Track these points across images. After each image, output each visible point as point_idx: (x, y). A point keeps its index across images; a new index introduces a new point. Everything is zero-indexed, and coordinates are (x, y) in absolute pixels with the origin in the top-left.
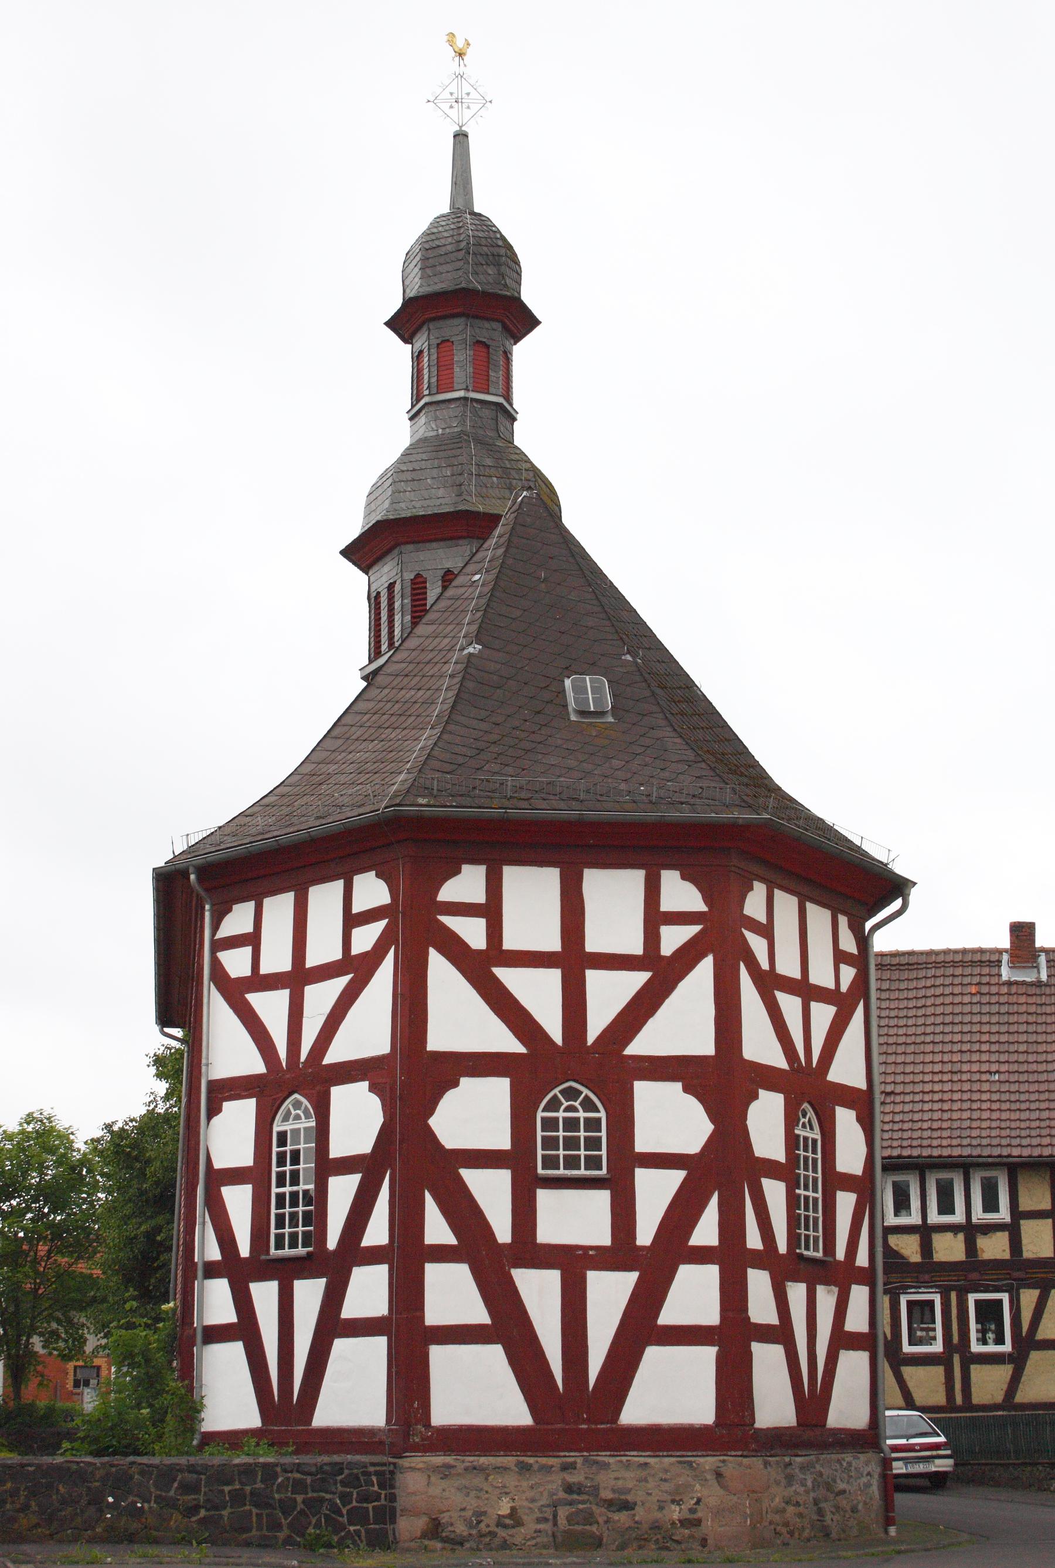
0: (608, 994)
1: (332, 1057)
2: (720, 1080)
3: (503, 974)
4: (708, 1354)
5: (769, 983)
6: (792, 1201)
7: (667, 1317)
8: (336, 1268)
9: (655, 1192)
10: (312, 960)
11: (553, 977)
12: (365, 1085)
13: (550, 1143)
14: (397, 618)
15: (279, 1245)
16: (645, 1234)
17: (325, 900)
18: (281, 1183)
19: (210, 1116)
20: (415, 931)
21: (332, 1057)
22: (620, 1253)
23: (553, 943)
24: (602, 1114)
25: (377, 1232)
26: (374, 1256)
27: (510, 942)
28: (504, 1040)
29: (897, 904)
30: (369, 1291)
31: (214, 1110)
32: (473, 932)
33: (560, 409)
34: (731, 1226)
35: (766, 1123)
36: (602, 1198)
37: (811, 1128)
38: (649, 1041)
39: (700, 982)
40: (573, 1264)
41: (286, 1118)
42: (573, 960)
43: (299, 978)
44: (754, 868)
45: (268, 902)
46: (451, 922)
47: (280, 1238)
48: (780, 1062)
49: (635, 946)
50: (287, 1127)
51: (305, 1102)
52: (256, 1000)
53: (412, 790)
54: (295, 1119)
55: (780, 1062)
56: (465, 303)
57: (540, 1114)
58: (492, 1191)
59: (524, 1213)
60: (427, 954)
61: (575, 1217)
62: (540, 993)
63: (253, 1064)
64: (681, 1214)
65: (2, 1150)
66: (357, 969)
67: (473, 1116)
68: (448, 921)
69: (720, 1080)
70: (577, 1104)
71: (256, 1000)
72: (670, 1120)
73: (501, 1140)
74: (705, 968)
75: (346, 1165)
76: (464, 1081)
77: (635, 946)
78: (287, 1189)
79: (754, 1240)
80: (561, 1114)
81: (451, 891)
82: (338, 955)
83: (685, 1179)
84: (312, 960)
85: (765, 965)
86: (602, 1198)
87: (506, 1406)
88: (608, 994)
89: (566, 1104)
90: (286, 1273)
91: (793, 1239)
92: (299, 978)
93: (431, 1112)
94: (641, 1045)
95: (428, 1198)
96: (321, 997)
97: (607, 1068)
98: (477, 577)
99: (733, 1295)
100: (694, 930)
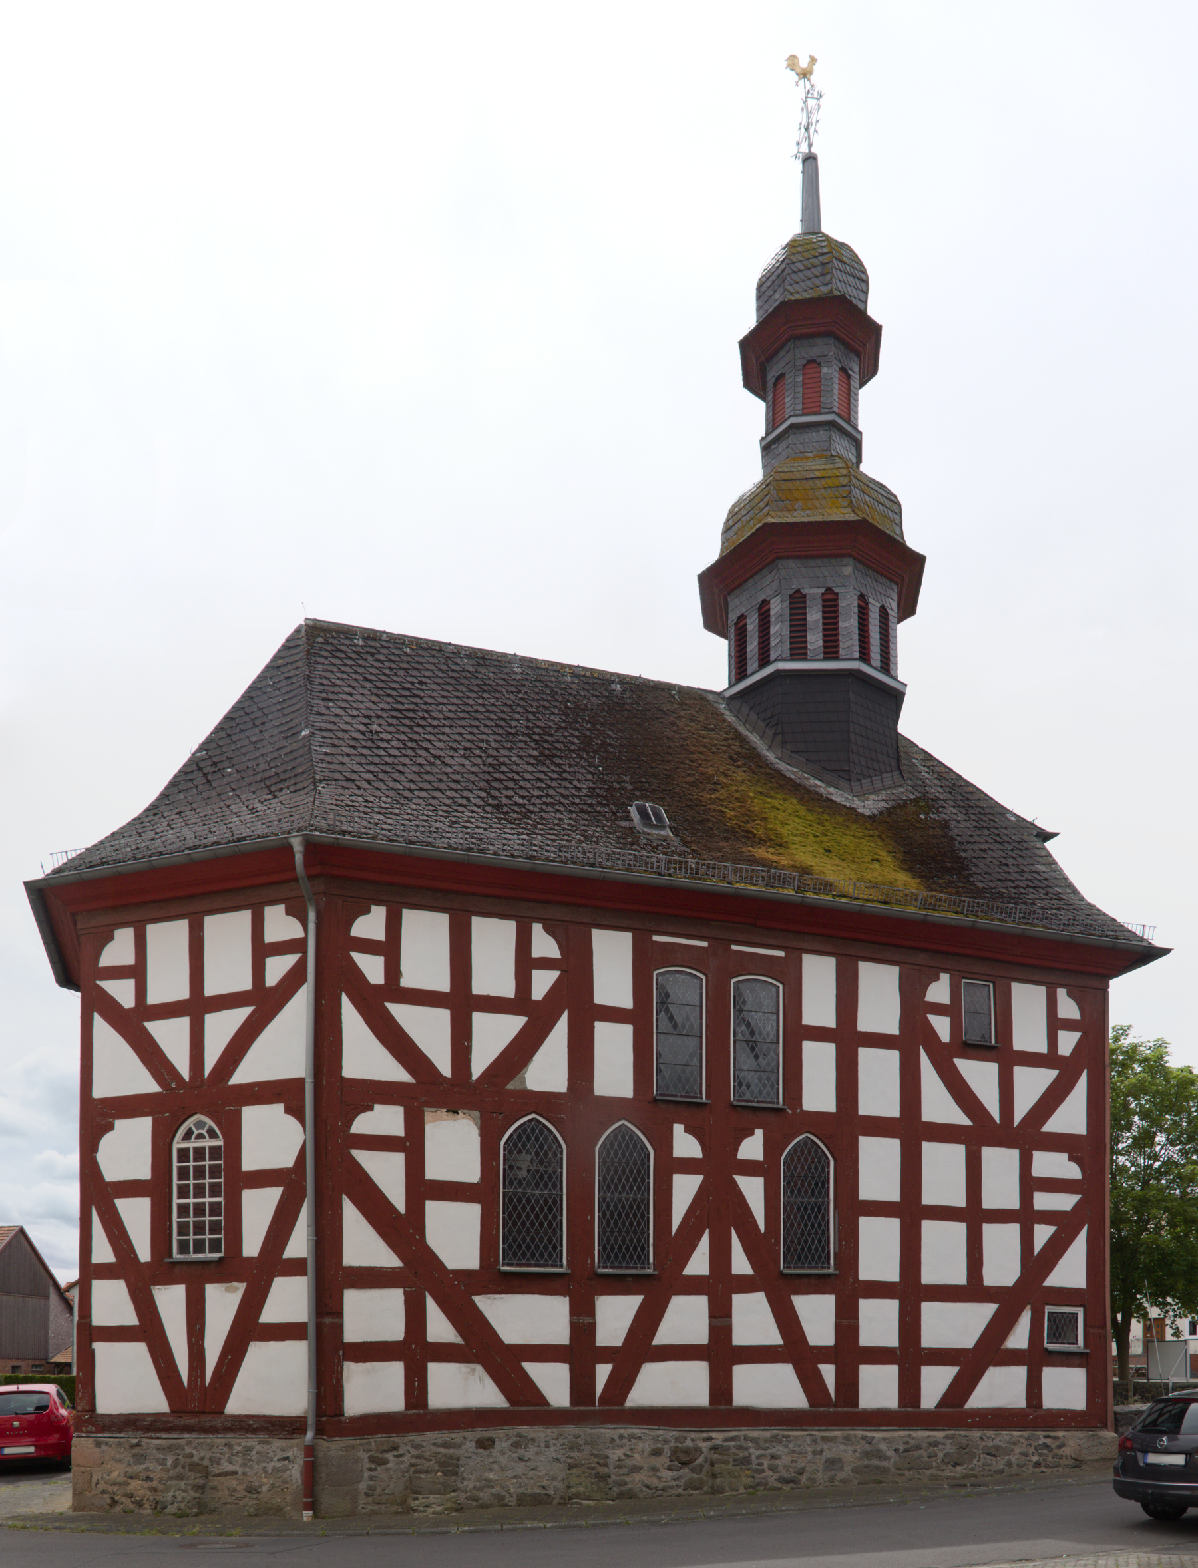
7: (664, 1336)
15: (184, 1247)
17: (228, 934)
18: (184, 1192)
25: (299, 1245)
26: (296, 1268)
30: (289, 1300)
33: (898, 434)
41: (188, 1135)
42: (461, 1002)
43: (197, 1006)
50: (192, 1144)
51: (210, 1123)
52: (156, 1028)
55: (150, 1086)
56: (812, 330)
62: (430, 1030)
65: (1191, 1139)
70: (204, 1132)
73: (143, 1171)
76: (377, 1107)
87: (154, 1400)
88: (492, 1035)
89: (196, 1132)
90: (195, 1280)
92: (197, 1006)
96: (221, 1028)
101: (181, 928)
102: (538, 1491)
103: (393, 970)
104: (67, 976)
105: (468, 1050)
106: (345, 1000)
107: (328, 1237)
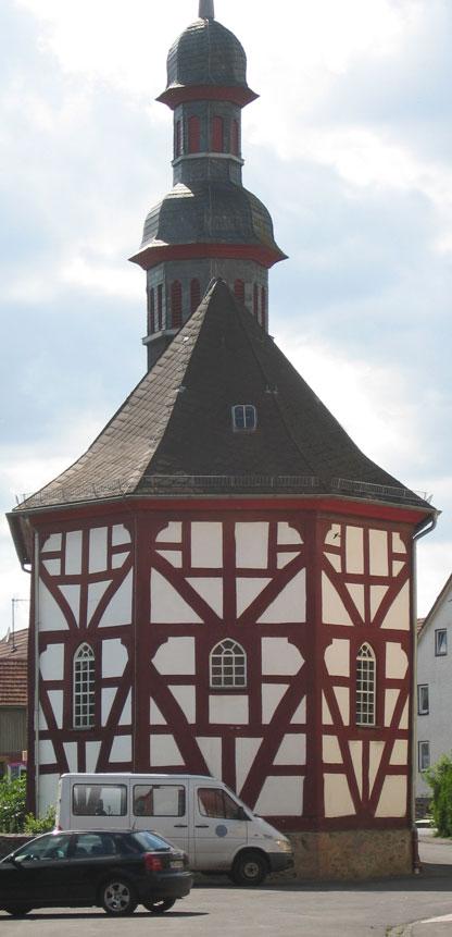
0: (248, 591)
1: (103, 624)
2: (310, 635)
3: (192, 581)
4: (299, 780)
5: (340, 580)
6: (354, 697)
7: (279, 760)
8: (106, 736)
9: (272, 696)
10: (92, 570)
11: (218, 582)
12: (119, 640)
13: (217, 671)
14: (164, 309)
15: (78, 723)
16: (267, 718)
17: (98, 536)
19: (40, 652)
20: (144, 558)
21: (103, 624)
22: (253, 728)
23: (218, 564)
24: (245, 656)
25: (126, 718)
26: (124, 730)
27: (195, 564)
28: (191, 616)
29: (430, 525)
31: (43, 649)
32: (175, 559)
34: (314, 713)
35: (337, 658)
36: (244, 700)
37: (370, 656)
38: (269, 617)
39: (299, 581)
40: (228, 734)
41: (80, 655)
43: (85, 579)
44: (332, 517)
45: (69, 535)
46: (163, 553)
47: (78, 719)
48: (348, 622)
49: (263, 565)
50: (81, 660)
52: (63, 588)
53: (142, 483)
54: (83, 657)
55: (348, 622)
56: (208, 80)
57: (211, 656)
58: (185, 697)
59: (202, 707)
60: (102, 628)
61: (229, 709)
62: (211, 591)
63: (63, 625)
64: (286, 707)
66: (115, 577)
67: (175, 657)
68: (160, 552)
69: (310, 635)
71: (63, 588)
72: (280, 657)
73: (189, 669)
74: (301, 576)
75: (110, 682)
76: (170, 639)
77: (263, 565)
78: (81, 694)
79: (327, 719)
80: (223, 656)
81: (162, 537)
82: (90, 586)
83: (288, 690)
84: (92, 570)
85: (338, 570)
86: (244, 700)
88: (248, 591)
89: (225, 650)
91: (354, 717)
92: (85, 579)
93: (153, 657)
94: (266, 618)
95: (152, 701)
96: (97, 591)
97: (248, 630)
98: (186, 338)
99: (314, 749)
100: (296, 554)
101: (105, 530)
102: (335, 834)
103: (187, 558)
104: (25, 557)
105: (391, 601)
106: (323, 574)
107: (141, 713)
